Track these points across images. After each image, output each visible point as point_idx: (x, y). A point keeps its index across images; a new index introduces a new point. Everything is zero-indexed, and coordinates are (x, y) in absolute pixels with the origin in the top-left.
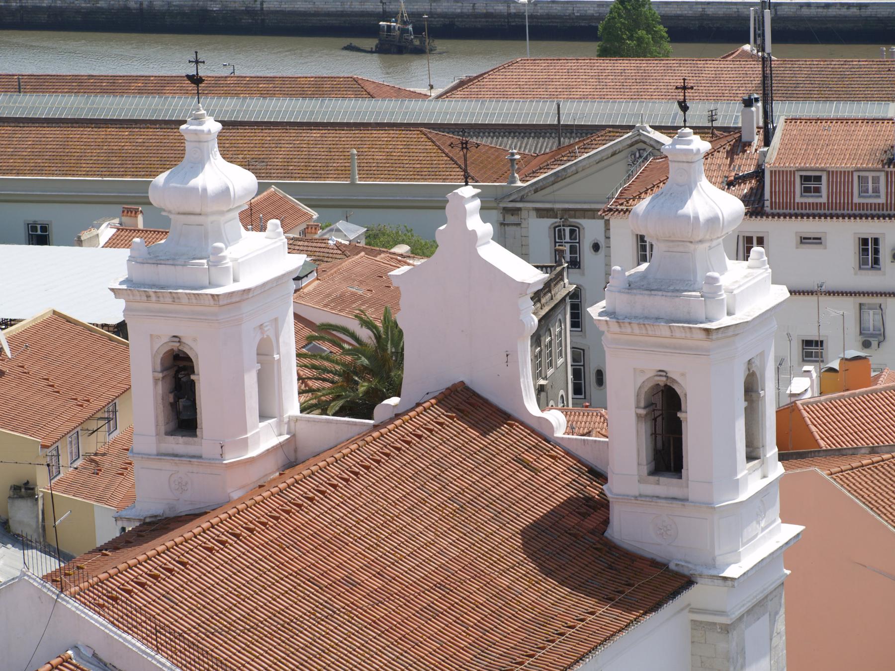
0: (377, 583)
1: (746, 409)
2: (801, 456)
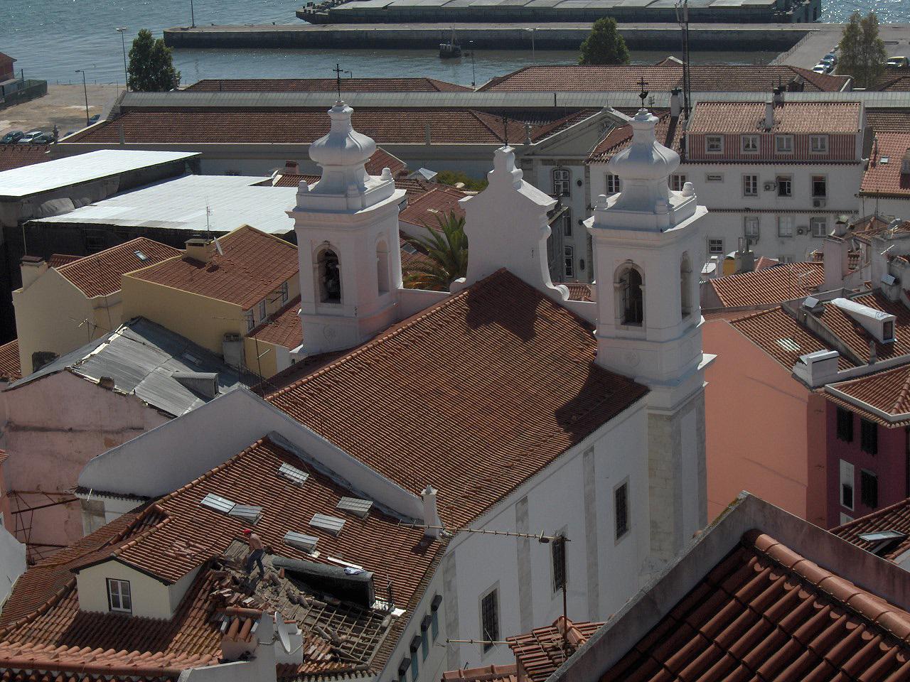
0: (455, 393)
1: (682, 283)
2: (713, 311)
